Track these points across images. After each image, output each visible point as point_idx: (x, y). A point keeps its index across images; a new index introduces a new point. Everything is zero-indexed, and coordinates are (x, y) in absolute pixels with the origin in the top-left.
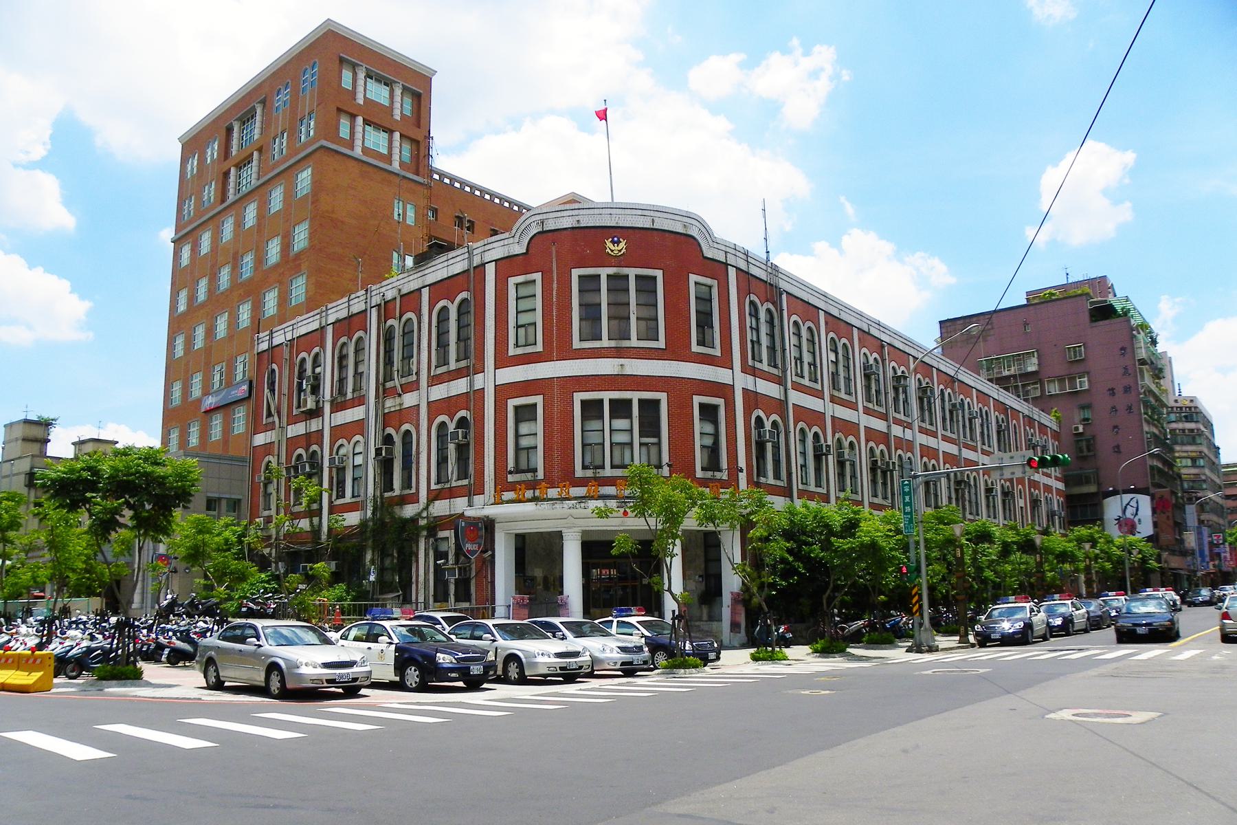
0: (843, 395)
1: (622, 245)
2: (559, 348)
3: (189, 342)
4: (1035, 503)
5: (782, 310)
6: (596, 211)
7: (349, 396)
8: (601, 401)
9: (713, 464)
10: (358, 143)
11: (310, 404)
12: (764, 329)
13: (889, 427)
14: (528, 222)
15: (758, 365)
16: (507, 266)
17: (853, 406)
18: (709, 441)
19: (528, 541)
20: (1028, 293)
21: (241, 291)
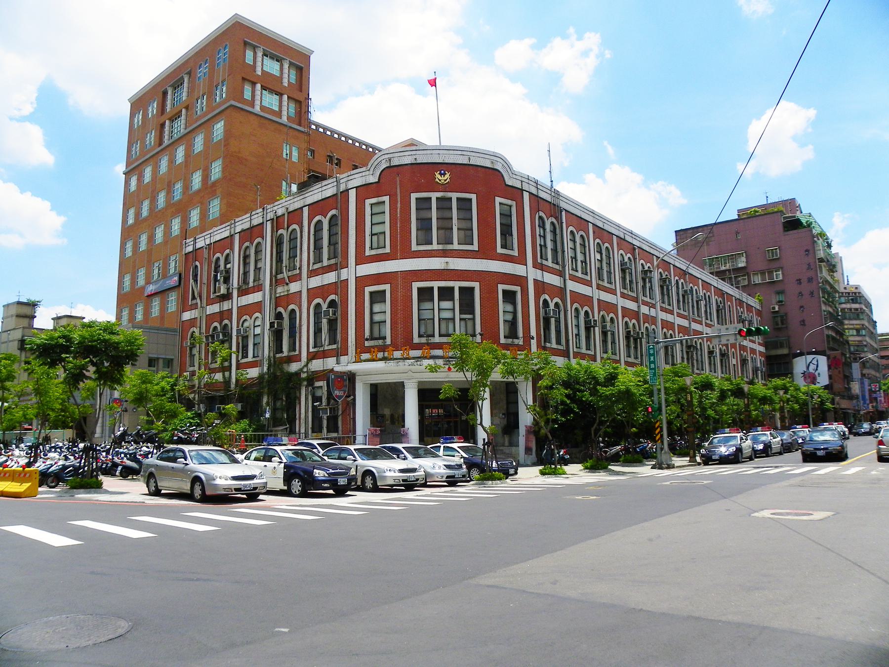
0: (606, 284)
1: (447, 176)
2: (402, 250)
3: (136, 246)
4: (744, 362)
5: (562, 223)
6: (428, 152)
7: (251, 284)
8: (432, 288)
9: (512, 333)
10: (258, 103)
11: (223, 290)
12: (549, 237)
13: (639, 307)
14: (379, 160)
15: (544, 262)
16: (365, 191)
17: (613, 292)
18: (509, 317)
19: (379, 389)
20: (739, 211)
21: (173, 209)
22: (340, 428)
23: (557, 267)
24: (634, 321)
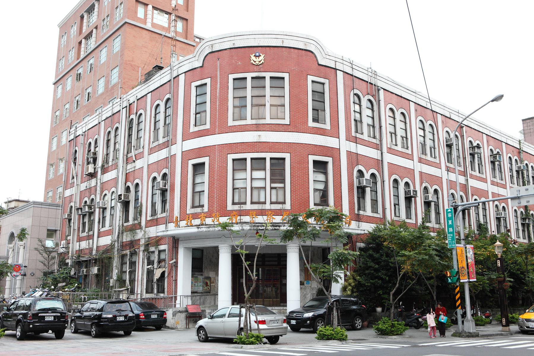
0: (429, 158)
1: (262, 58)
3: (59, 141)
5: (379, 101)
7: (110, 164)
10: (149, 20)
11: (91, 170)
14: (203, 47)
19: (205, 253)
21: (85, 110)
22: (166, 290)
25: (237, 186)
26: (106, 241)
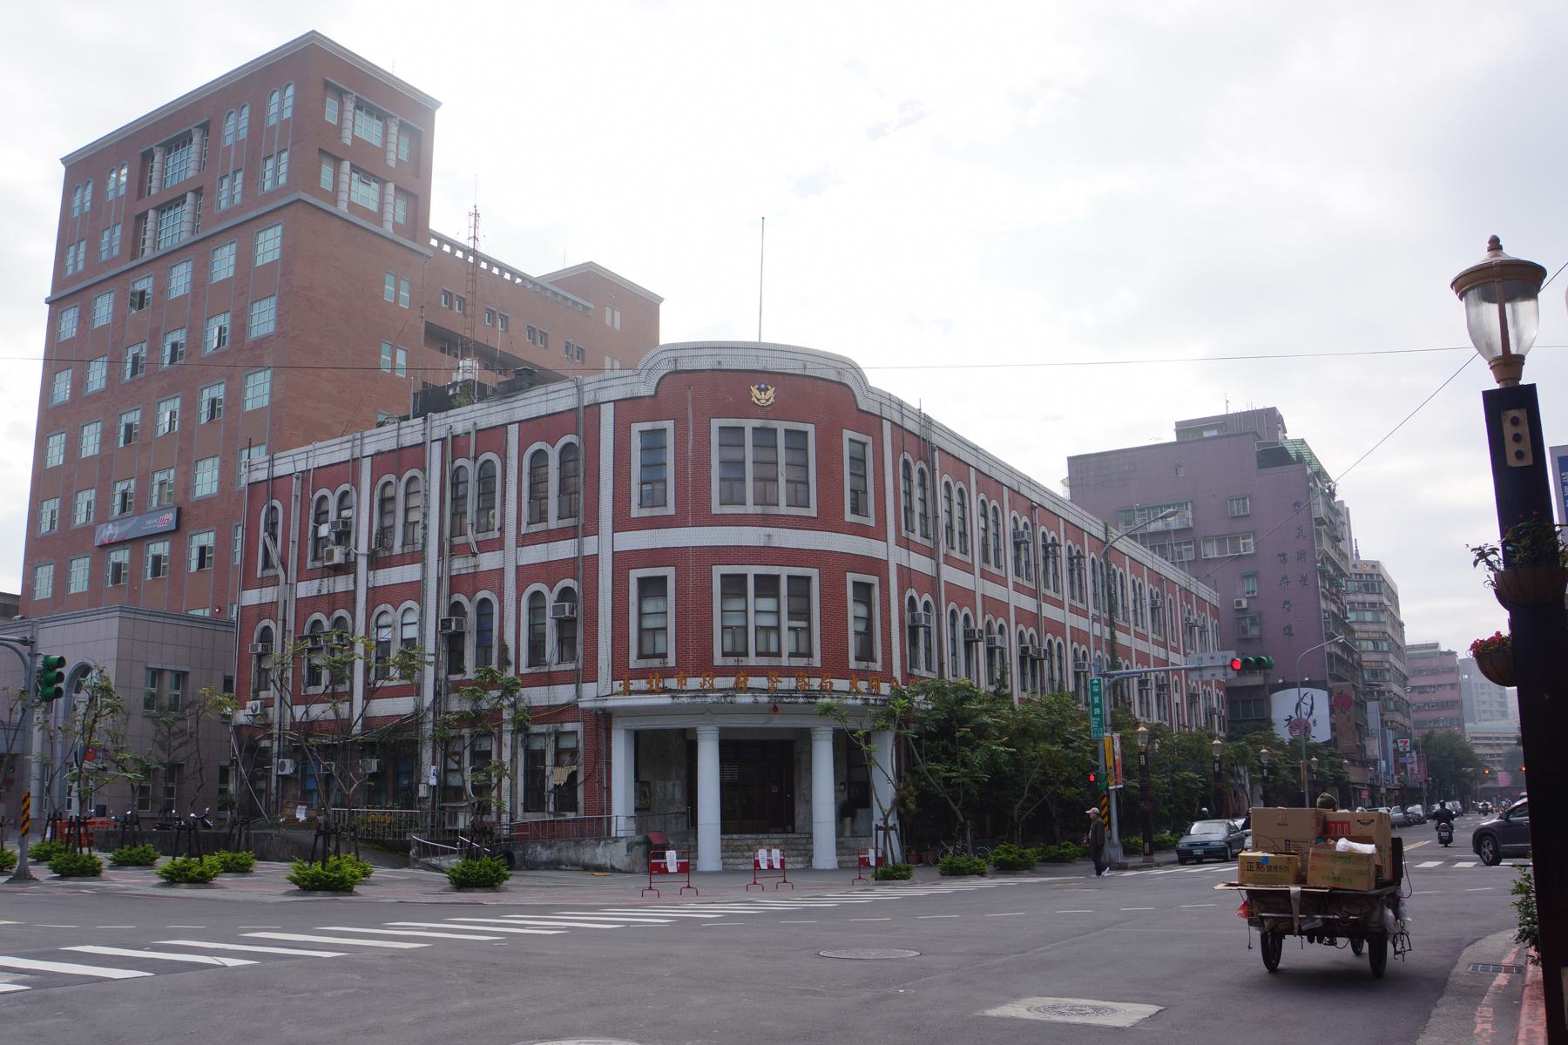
0: (993, 570)
1: (770, 393)
2: (694, 512)
4: (1193, 698)
6: (740, 352)
7: (397, 549)
8: (744, 576)
9: (866, 654)
10: (343, 196)
11: (338, 557)
12: (917, 493)
13: (1039, 606)
14: (656, 359)
15: (911, 536)
16: (628, 409)
17: (1002, 581)
18: (861, 627)
23: (927, 543)
24: (927, 597)
25: (728, 623)
26: (403, 706)
